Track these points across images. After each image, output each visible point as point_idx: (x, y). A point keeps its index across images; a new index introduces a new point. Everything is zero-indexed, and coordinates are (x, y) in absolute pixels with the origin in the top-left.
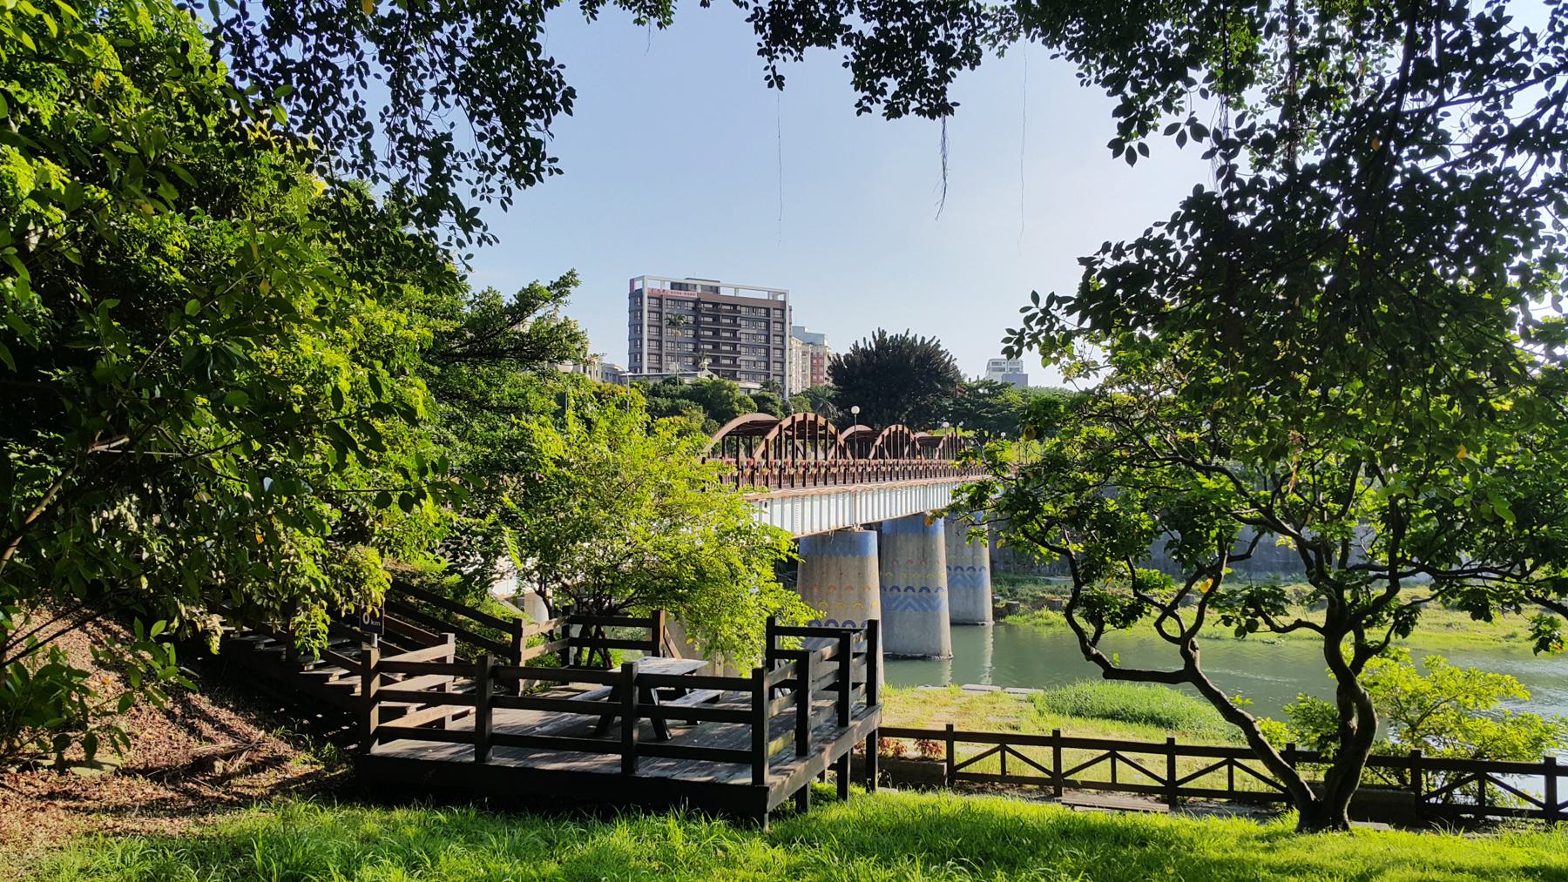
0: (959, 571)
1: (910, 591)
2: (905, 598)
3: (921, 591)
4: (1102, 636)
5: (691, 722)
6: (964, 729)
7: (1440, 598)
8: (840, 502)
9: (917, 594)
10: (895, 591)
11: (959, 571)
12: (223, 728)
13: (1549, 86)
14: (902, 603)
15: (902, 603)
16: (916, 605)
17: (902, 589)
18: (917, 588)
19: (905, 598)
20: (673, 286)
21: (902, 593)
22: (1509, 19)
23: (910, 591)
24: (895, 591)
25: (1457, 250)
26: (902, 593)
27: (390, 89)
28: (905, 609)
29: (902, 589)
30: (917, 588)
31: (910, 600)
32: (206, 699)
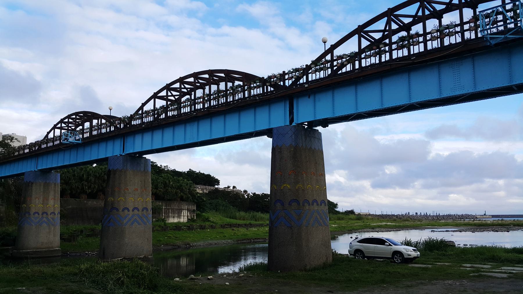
0: (45, 215)
1: (136, 211)
4: (391, 6)
6: (455, 41)
7: (127, 188)
8: (94, 133)
9: (140, 213)
10: (126, 211)
11: (45, 215)
17: (131, 209)
18: (140, 208)
19: (132, 217)
20: (464, 245)
21: (131, 213)
23: (136, 211)
24: (126, 211)
25: (517, 12)
26: (131, 213)
28: (132, 223)
29: (131, 209)
30: (140, 208)
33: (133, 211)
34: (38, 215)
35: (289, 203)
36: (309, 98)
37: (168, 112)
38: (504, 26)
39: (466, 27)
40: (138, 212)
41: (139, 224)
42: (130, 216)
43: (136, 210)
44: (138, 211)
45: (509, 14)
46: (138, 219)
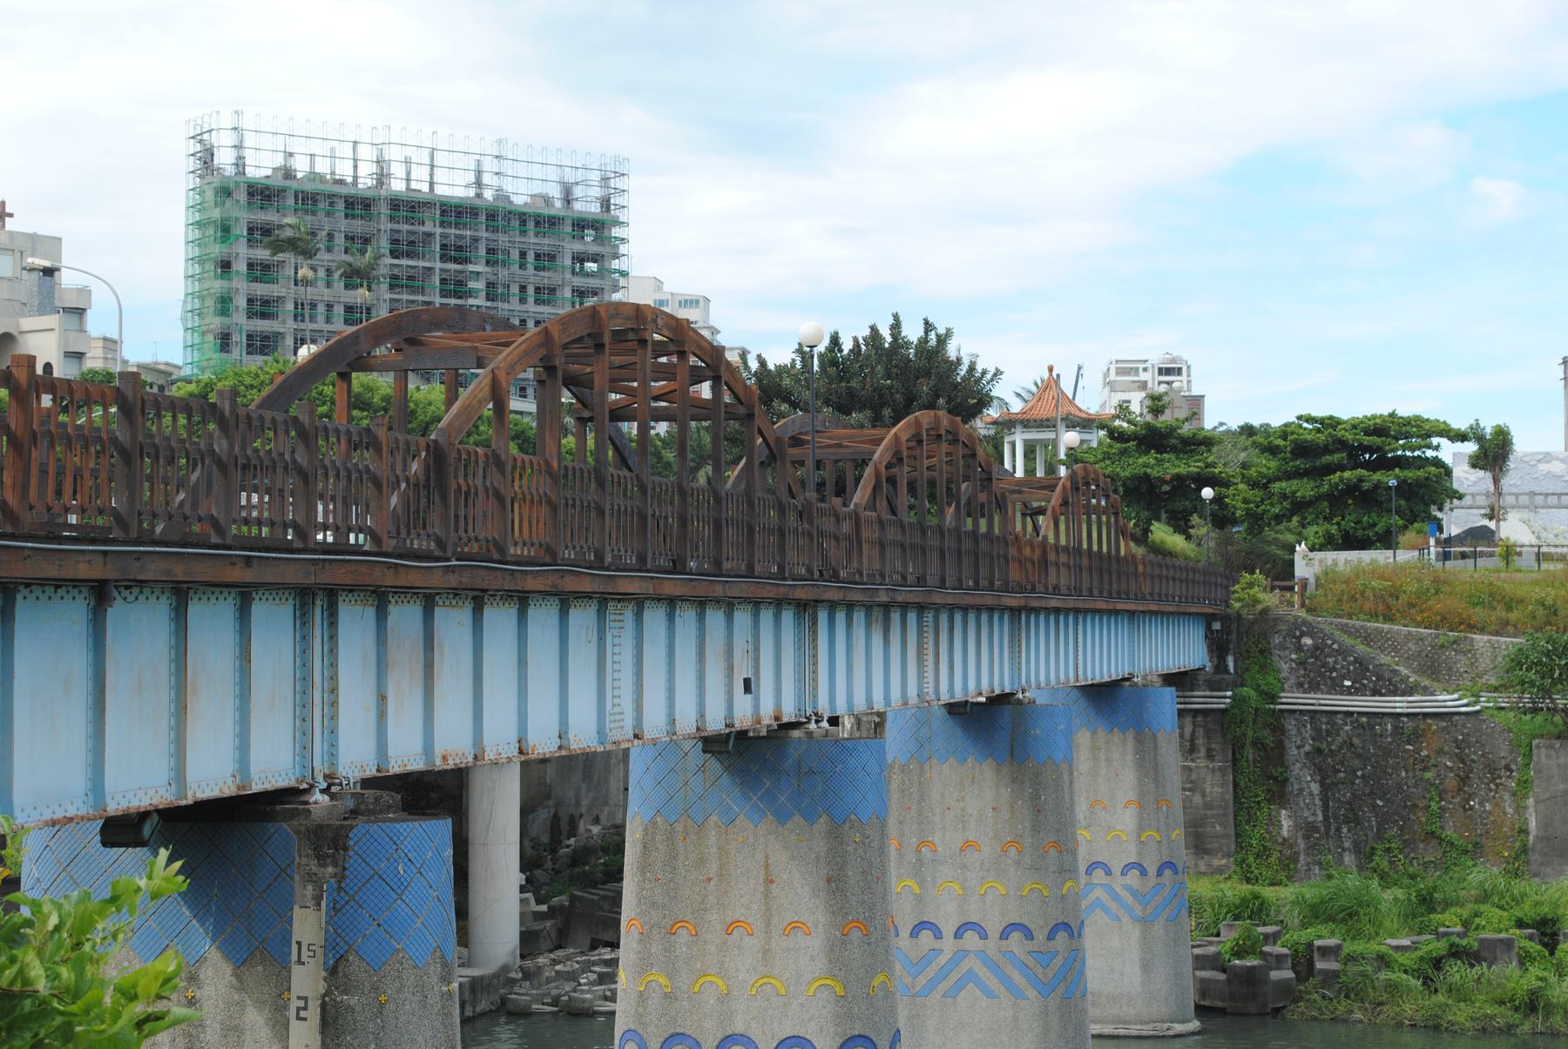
0: (1099, 874)
1: (971, 938)
2: (961, 954)
3: (1004, 935)
5: (1369, 718)
9: (992, 945)
10: (926, 936)
12: (612, 505)
13: (591, 451)
14: (944, 973)
15: (944, 973)
16: (992, 982)
17: (948, 929)
19: (961, 954)
21: (948, 944)
22: (873, 329)
23: (971, 938)
26: (948, 944)
27: (1386, 414)
28: (959, 987)
29: (948, 929)
30: (994, 926)
31: (1099, 893)
32: (143, 377)
33: (958, 935)
34: (1106, 874)
35: (860, 1036)
36: (250, 567)
37: (1173, 616)
38: (41, 389)
39: (1164, 573)
40: (982, 942)
41: (990, 994)
42: (943, 959)
43: (969, 933)
44: (984, 936)
45: (1191, 576)
46: (982, 971)
